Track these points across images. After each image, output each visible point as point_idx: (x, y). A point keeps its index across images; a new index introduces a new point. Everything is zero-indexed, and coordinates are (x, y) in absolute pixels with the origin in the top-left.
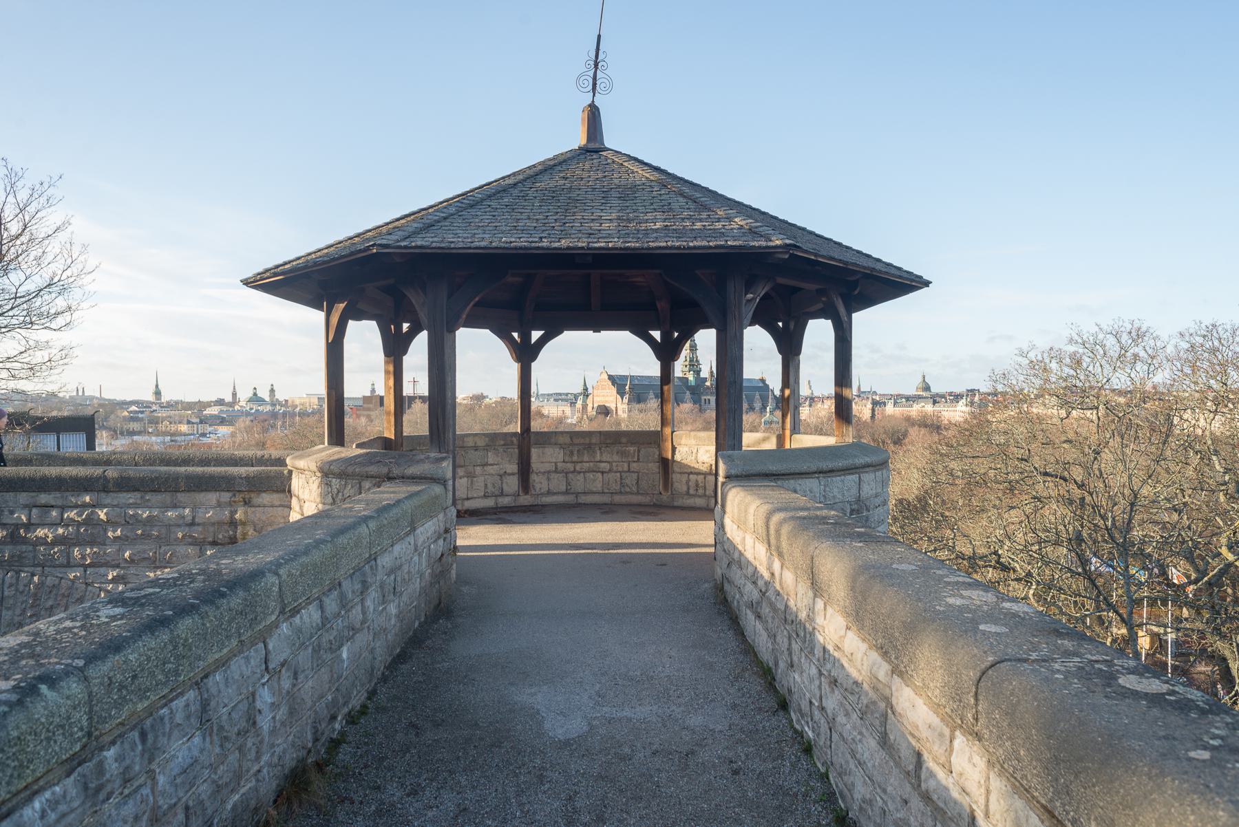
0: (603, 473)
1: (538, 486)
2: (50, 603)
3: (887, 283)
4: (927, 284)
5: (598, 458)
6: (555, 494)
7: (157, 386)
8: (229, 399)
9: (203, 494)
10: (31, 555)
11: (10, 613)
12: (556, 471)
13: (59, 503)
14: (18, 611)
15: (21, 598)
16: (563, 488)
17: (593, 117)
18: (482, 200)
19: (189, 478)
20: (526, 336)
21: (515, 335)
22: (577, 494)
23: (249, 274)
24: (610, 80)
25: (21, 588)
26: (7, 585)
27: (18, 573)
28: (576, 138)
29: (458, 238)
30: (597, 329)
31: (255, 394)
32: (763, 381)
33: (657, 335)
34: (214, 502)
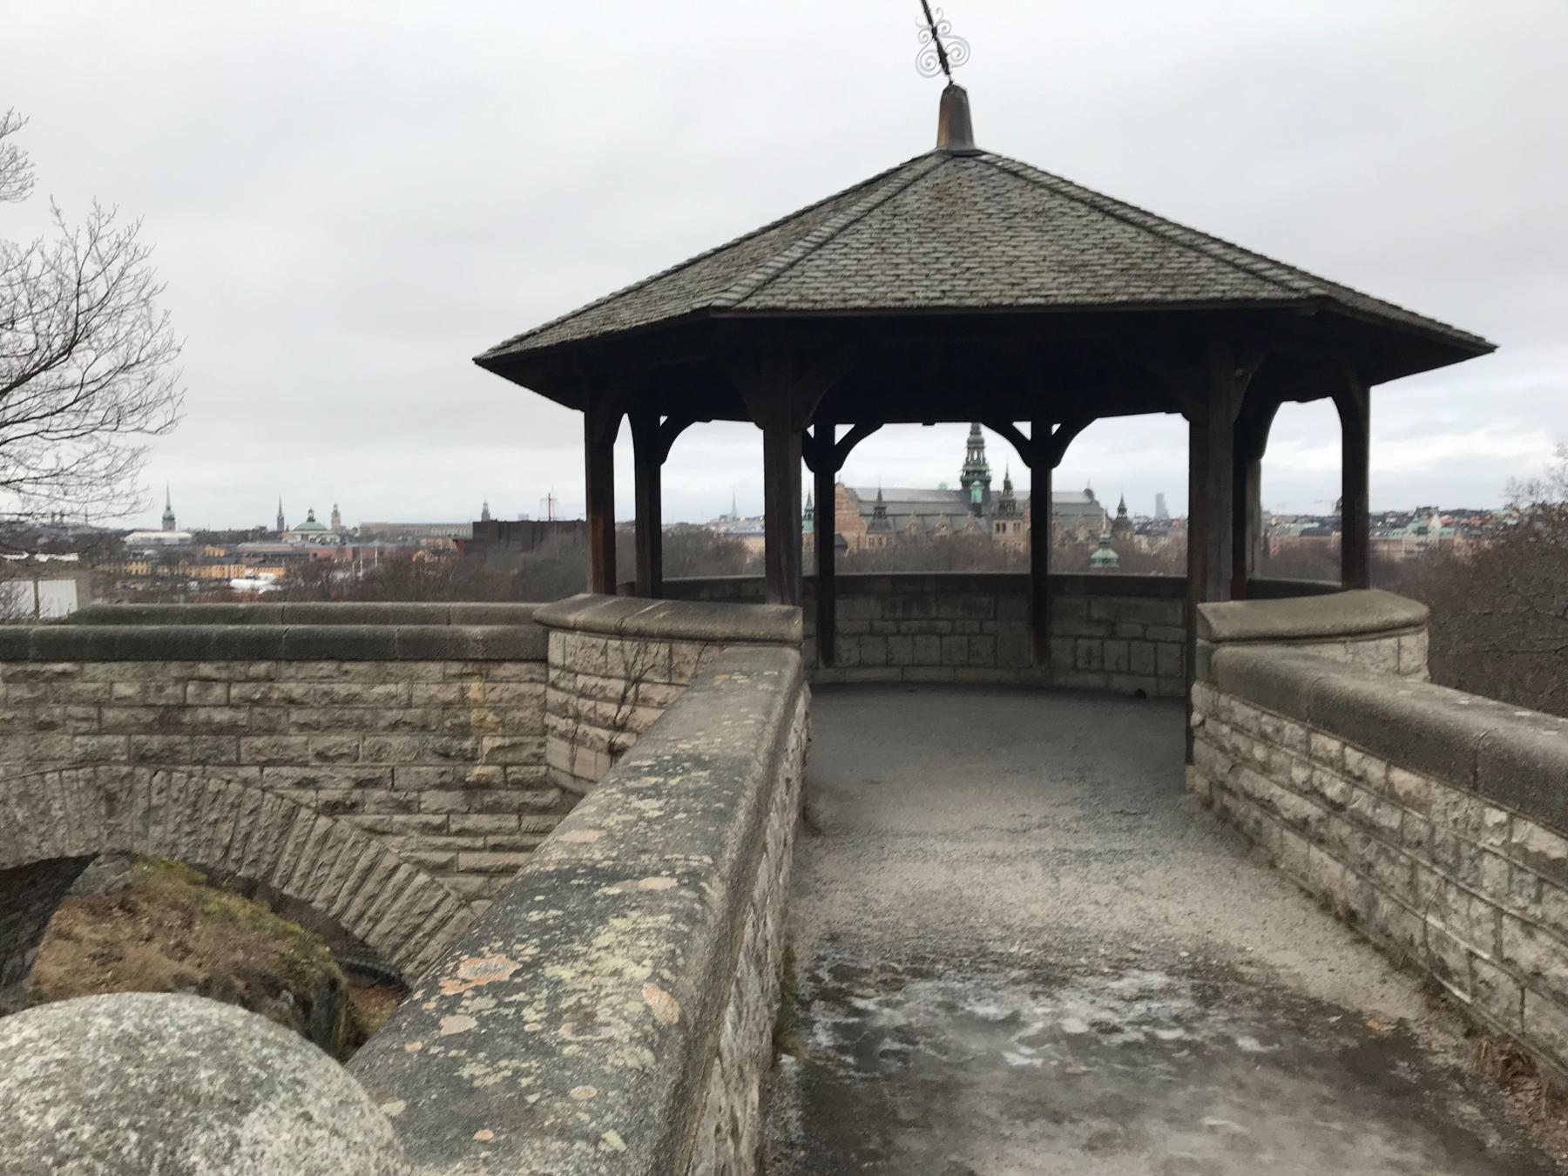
0: (941, 636)
1: (845, 655)
2: (214, 816)
3: (1432, 346)
4: (1490, 349)
5: (933, 614)
6: (869, 666)
7: (168, 508)
8: (272, 526)
9: (421, 665)
10: (187, 748)
11: (160, 829)
12: (872, 633)
13: (224, 675)
14: (171, 827)
15: (175, 809)
16: (882, 658)
17: (954, 105)
18: (833, 237)
19: (405, 640)
20: (826, 432)
21: (811, 430)
22: (903, 667)
23: (482, 350)
24: (962, 41)
25: (175, 795)
26: (154, 791)
27: (170, 773)
28: (921, 136)
29: (826, 285)
30: (928, 422)
31: (311, 519)
32: (1089, 493)
33: (1025, 428)
34: (439, 676)
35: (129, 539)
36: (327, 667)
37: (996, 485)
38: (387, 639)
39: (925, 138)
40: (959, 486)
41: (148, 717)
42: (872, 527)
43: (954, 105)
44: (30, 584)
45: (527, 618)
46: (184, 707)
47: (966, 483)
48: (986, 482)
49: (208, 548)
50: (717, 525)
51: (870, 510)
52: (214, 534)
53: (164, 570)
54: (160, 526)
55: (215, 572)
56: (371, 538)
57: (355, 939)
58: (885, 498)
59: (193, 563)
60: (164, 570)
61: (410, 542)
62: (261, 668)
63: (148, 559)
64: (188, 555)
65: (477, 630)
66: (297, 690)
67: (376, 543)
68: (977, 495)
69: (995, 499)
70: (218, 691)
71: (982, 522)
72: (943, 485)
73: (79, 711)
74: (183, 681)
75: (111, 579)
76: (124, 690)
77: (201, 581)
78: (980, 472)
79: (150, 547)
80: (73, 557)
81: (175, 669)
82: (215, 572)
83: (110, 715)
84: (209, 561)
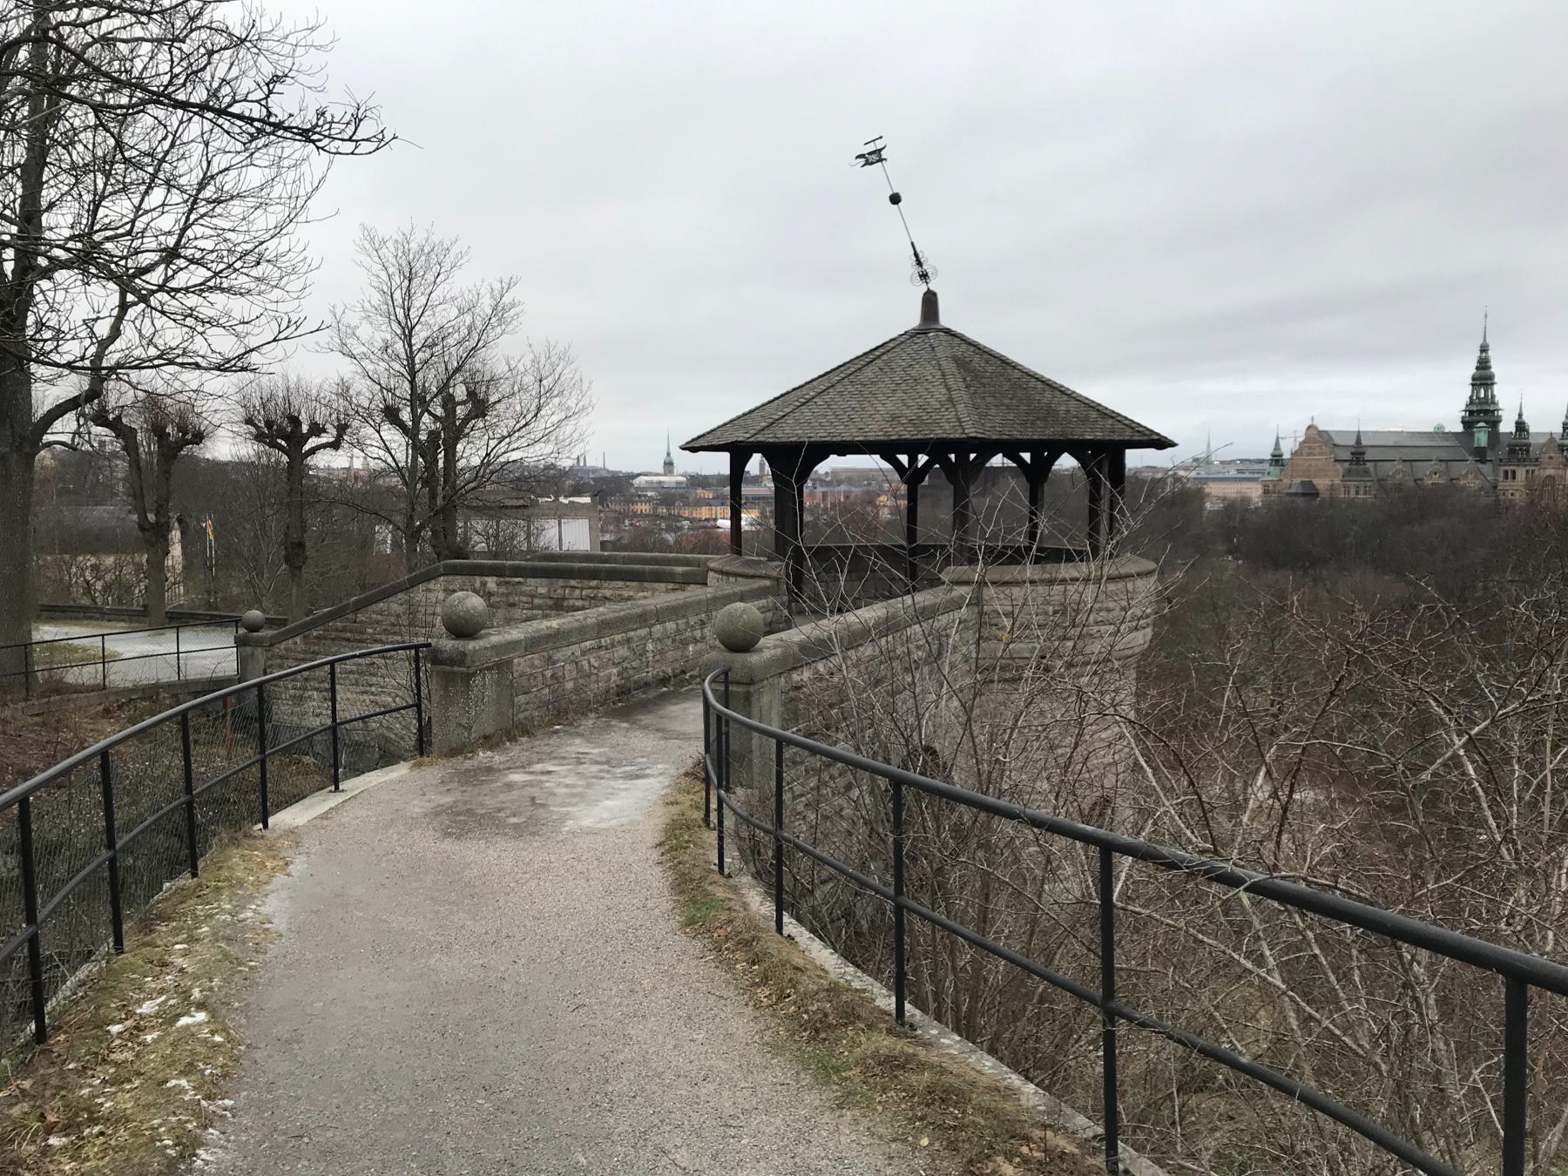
17: (930, 303)
35: (636, 482)
36: (621, 584)
37: (1507, 426)
38: (643, 572)
39: (913, 319)
40: (1459, 428)
41: (551, 602)
42: (1348, 472)
43: (930, 303)
44: (554, 523)
45: (698, 563)
46: (564, 599)
47: (1468, 424)
48: (1494, 423)
49: (700, 491)
50: (1186, 469)
51: (1347, 455)
52: (706, 477)
53: (663, 511)
54: (661, 471)
55: (704, 513)
56: (840, 483)
57: (361, 499)
58: (1364, 442)
59: (687, 504)
60: (663, 511)
61: (874, 486)
62: (594, 583)
63: (650, 500)
64: (683, 497)
65: (680, 569)
66: (608, 593)
67: (843, 488)
68: (1482, 438)
69: (1504, 441)
70: (577, 592)
71: (1486, 468)
72: (1440, 427)
73: (524, 599)
74: (564, 587)
75: (619, 518)
76: (542, 590)
77: (692, 520)
78: (1486, 412)
79: (653, 489)
80: (587, 500)
81: (561, 582)
82: (704, 513)
83: (536, 601)
84: (699, 503)
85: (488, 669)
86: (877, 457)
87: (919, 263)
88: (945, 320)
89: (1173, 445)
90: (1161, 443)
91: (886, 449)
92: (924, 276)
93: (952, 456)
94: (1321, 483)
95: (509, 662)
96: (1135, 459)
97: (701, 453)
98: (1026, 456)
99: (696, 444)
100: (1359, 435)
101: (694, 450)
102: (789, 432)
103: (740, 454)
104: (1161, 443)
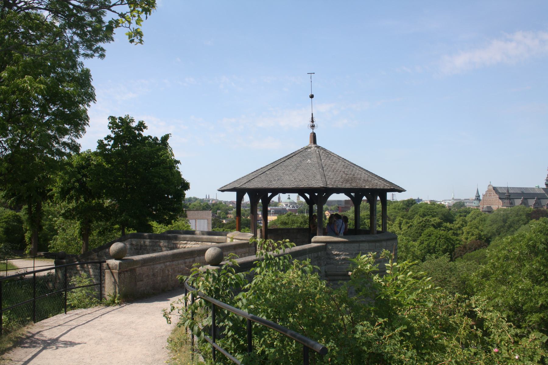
62: (185, 242)
85: (127, 271)
86: (343, 194)
87: (313, 121)
88: (319, 143)
89: (405, 191)
90: (400, 190)
91: (301, 191)
92: (313, 126)
93: (316, 194)
94: (494, 207)
95: (134, 269)
96: (389, 196)
97: (225, 192)
98: (308, 196)
99: (223, 189)
100: (508, 189)
101: (223, 191)
102: (256, 184)
103: (240, 193)
104: (400, 190)
